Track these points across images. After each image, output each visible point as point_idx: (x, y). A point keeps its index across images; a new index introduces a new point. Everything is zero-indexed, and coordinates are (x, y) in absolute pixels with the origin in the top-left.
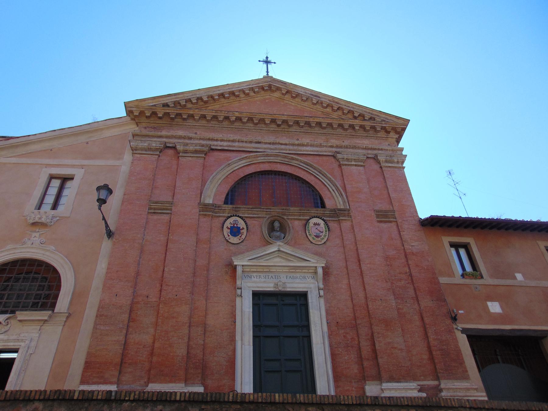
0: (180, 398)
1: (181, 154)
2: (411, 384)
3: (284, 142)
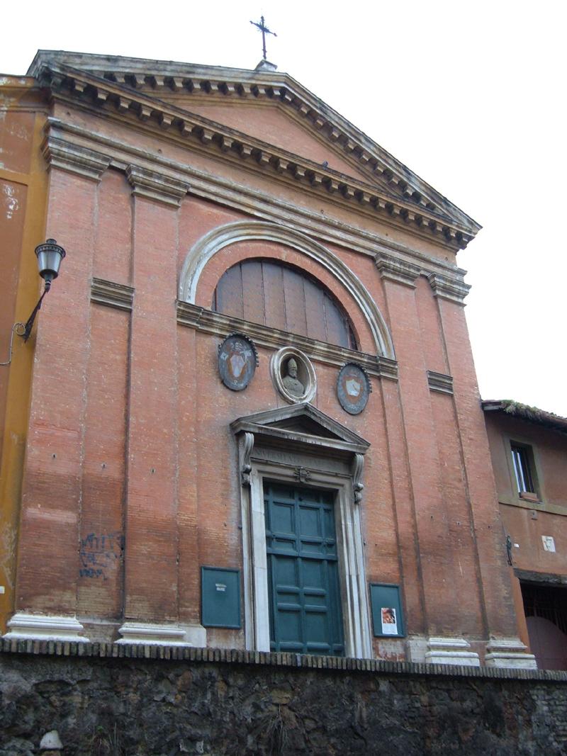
0: (260, 661)
1: (137, 190)
2: (444, 661)
3: (438, 262)
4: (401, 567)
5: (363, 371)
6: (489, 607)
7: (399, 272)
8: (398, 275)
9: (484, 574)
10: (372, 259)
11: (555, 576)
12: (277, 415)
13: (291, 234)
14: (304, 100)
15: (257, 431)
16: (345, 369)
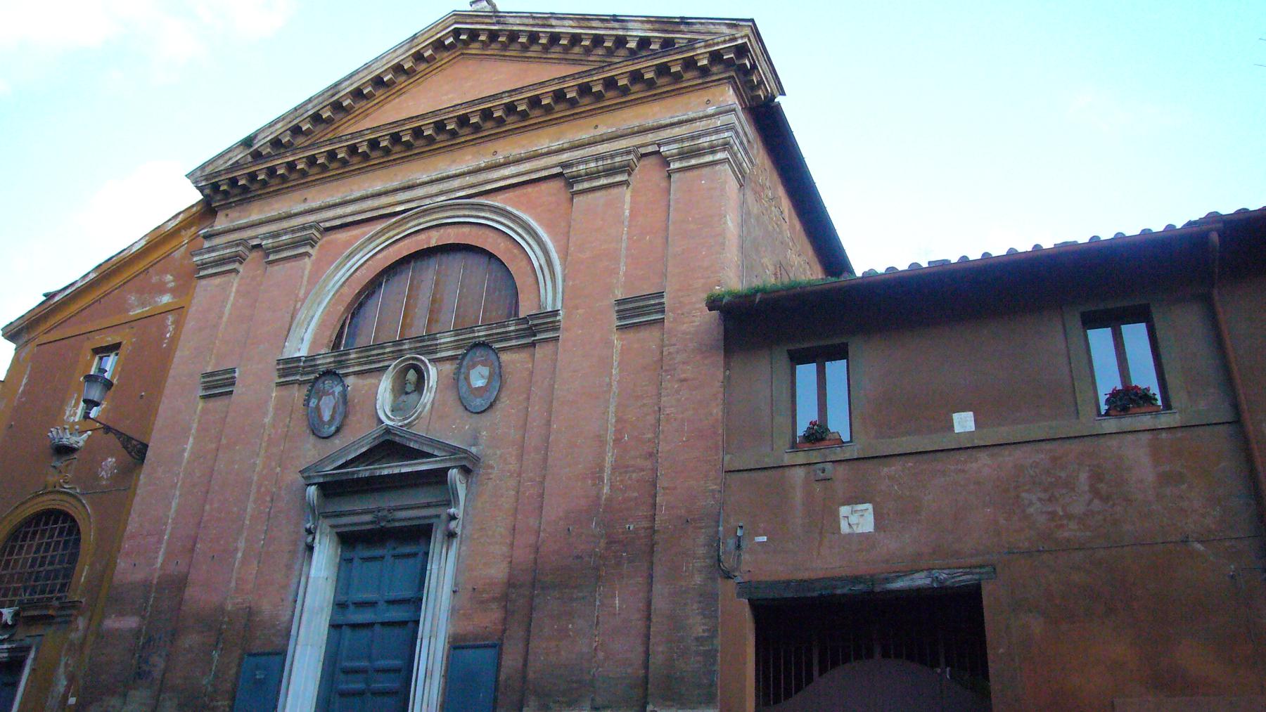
3: (676, 120)
4: (508, 614)
5: (335, 373)
6: (657, 660)
7: (599, 172)
8: (599, 177)
9: (659, 604)
10: (560, 175)
11: (856, 579)
12: (349, 453)
13: (442, 208)
14: (478, 27)
15: (321, 480)
16: (468, 358)
